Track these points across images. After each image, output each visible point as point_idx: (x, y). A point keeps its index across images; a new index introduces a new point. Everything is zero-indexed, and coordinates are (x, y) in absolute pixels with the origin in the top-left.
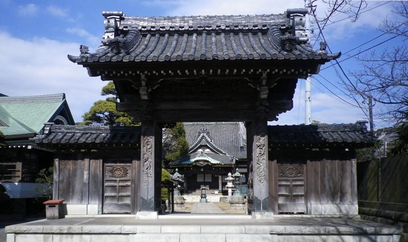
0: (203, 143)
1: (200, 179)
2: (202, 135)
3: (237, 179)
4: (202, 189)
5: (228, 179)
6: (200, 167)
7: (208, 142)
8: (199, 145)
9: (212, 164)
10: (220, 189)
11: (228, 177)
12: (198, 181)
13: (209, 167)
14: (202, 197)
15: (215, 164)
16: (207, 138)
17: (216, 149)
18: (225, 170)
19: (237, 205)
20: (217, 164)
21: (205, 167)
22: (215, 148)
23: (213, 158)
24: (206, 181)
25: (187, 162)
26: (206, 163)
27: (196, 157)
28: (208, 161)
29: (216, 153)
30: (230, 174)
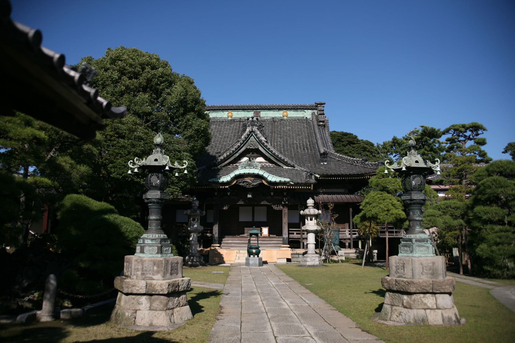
0: (252, 143)
1: (244, 217)
2: (248, 130)
3: (415, 181)
4: (251, 235)
5: (307, 211)
6: (245, 190)
7: (260, 142)
8: (243, 149)
9: (270, 183)
10: (285, 235)
11: (307, 207)
12: (241, 220)
13: (263, 190)
14: (250, 254)
15: (275, 183)
16: (260, 135)
17: (276, 157)
18: (295, 197)
19: (429, 300)
20: (280, 183)
21: (255, 190)
22: (273, 155)
23: (271, 172)
24: (256, 220)
25: (214, 180)
26: (259, 182)
27: (237, 168)
28: (261, 177)
29: (276, 164)
30: (310, 202)
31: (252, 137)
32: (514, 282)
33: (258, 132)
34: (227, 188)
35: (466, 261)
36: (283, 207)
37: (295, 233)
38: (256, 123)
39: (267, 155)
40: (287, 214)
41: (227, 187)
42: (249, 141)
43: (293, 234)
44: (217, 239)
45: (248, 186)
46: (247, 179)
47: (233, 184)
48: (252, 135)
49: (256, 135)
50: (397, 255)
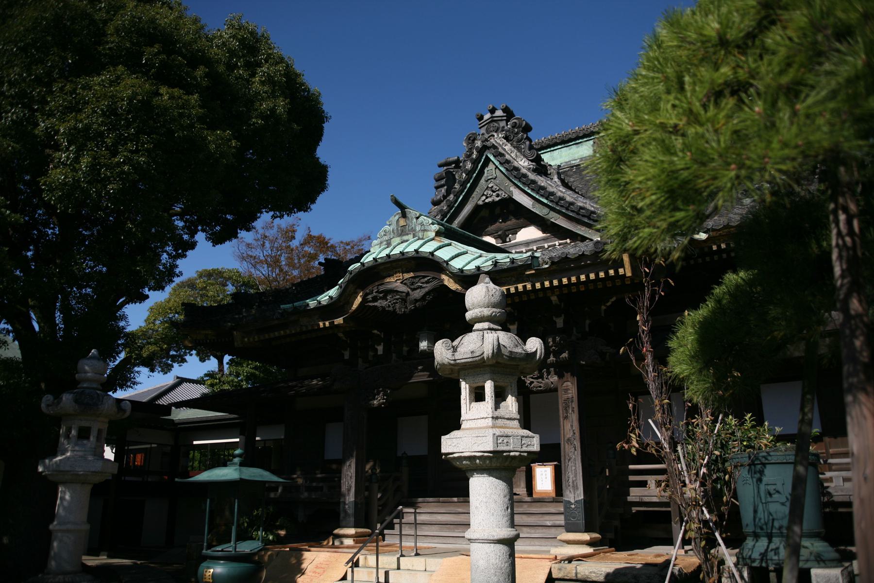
7: (514, 174)
31: (491, 166)
32: (503, 578)
33: (508, 147)
34: (338, 326)
35: (726, 183)
36: (561, 376)
37: (651, 480)
38: (503, 124)
39: (539, 210)
40: (575, 405)
41: (339, 321)
42: (483, 181)
43: (644, 484)
44: (351, 511)
45: (400, 309)
46: (395, 282)
47: (355, 306)
48: (488, 160)
49: (498, 155)
50: (458, 427)
